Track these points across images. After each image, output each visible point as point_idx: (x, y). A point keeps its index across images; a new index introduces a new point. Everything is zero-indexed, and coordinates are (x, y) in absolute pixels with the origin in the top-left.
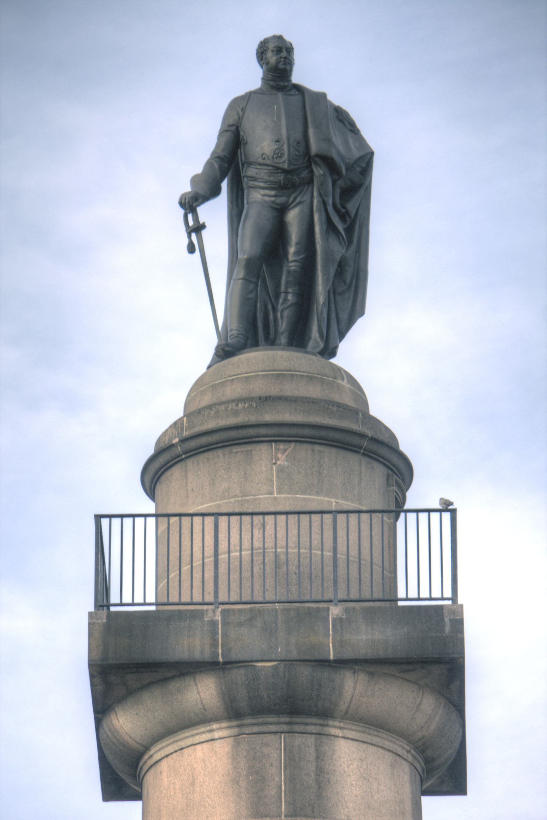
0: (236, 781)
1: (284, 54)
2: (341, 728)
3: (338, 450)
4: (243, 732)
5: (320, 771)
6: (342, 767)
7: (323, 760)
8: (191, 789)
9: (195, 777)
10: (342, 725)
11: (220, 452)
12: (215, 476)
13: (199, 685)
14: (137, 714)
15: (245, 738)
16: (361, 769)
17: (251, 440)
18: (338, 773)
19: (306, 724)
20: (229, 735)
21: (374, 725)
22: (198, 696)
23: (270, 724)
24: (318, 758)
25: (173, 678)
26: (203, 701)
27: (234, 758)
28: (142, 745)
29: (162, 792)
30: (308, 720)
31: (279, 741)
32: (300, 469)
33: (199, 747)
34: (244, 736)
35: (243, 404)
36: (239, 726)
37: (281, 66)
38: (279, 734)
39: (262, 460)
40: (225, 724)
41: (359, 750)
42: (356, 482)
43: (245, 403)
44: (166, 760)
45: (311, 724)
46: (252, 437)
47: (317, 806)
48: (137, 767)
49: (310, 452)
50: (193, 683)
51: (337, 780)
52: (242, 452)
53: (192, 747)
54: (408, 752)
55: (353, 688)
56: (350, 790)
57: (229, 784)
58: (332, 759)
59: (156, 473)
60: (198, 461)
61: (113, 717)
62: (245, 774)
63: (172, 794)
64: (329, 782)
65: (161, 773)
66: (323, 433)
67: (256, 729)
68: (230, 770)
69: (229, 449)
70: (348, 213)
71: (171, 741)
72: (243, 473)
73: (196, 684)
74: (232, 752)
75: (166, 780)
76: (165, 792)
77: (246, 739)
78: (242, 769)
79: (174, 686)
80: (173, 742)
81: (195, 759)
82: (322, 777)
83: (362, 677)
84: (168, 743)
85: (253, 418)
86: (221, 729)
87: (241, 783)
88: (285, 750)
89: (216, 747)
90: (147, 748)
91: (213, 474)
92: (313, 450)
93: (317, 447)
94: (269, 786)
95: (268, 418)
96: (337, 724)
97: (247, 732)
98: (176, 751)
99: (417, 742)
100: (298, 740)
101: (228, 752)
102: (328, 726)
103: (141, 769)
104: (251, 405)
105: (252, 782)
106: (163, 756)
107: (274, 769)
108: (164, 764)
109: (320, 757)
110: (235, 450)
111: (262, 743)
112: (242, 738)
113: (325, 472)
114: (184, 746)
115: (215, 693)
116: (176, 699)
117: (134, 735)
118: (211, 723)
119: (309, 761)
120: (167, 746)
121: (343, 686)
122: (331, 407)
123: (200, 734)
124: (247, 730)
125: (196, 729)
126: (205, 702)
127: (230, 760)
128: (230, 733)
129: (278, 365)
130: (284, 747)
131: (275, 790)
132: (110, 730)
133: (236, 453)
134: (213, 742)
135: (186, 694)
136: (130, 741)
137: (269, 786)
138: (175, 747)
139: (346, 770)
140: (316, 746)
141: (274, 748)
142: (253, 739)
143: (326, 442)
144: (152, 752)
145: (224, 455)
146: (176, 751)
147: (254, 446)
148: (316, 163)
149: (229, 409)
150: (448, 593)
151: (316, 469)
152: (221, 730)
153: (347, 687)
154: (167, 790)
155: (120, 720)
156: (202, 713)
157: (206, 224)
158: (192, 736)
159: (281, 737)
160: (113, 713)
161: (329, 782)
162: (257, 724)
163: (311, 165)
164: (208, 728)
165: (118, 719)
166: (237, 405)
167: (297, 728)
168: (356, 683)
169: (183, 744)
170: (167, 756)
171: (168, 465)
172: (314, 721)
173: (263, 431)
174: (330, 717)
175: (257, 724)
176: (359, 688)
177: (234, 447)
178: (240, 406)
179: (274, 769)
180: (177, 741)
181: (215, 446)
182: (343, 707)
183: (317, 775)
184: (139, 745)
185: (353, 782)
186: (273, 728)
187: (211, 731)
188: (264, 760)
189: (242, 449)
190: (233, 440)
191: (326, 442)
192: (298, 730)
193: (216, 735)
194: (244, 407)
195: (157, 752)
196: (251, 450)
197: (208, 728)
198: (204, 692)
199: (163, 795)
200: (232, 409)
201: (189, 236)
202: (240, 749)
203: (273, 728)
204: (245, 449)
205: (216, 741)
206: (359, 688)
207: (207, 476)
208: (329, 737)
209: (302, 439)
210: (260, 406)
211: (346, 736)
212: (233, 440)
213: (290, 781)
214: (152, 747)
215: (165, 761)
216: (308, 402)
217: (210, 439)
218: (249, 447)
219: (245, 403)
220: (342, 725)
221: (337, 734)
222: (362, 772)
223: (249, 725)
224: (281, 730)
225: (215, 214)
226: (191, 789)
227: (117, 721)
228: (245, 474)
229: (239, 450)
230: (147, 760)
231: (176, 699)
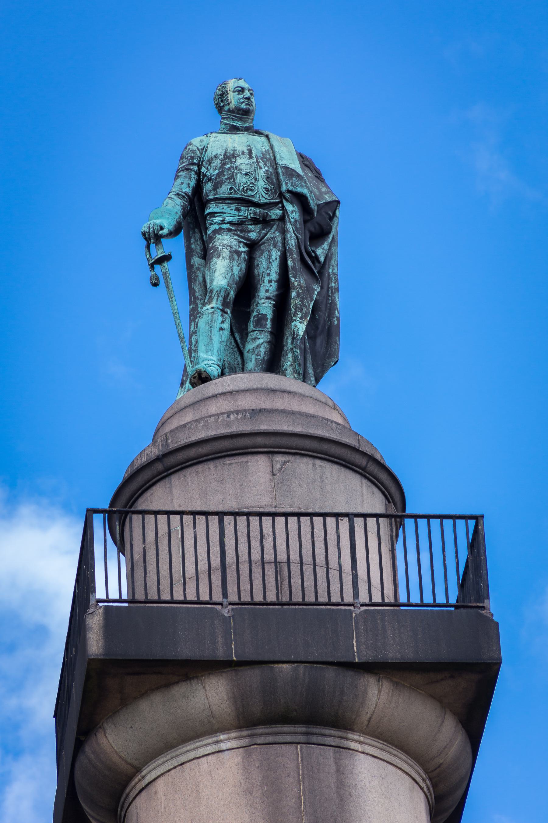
0: (249, 792)
1: (247, 94)
2: (360, 742)
3: (339, 467)
4: (255, 742)
5: (341, 784)
6: (363, 783)
7: (343, 773)
8: (196, 802)
9: (201, 791)
10: (362, 739)
11: (211, 465)
12: (206, 489)
13: (208, 688)
14: (131, 727)
15: (257, 748)
16: (382, 787)
17: (246, 451)
18: (359, 787)
19: (324, 735)
20: (239, 746)
21: (394, 740)
22: (206, 701)
23: (285, 733)
24: (338, 771)
25: (177, 683)
26: (211, 707)
27: (246, 770)
28: (133, 766)
29: (158, 812)
30: (327, 731)
31: (295, 752)
32: (301, 483)
33: (203, 760)
34: (255, 746)
35: (236, 416)
36: (249, 736)
37: (243, 106)
38: (295, 745)
39: (259, 472)
40: (234, 735)
41: (379, 767)
42: (359, 503)
43: (238, 414)
44: (162, 778)
45: (331, 736)
46: (247, 448)
47: (340, 819)
48: (120, 798)
49: (311, 466)
50: (200, 687)
51: (359, 795)
52: (236, 463)
53: (195, 761)
54: (424, 780)
55: (377, 697)
56: (372, 806)
57: (241, 795)
58: (352, 773)
59: (132, 496)
60: (185, 476)
61: (100, 736)
62: (259, 784)
63: (172, 811)
64: (351, 796)
65: (156, 793)
66: (325, 447)
67: (270, 739)
68: (242, 781)
69: (221, 461)
70: (315, 259)
71: (169, 757)
72: (238, 485)
73: (204, 688)
74: (243, 762)
75: (163, 798)
76: (163, 810)
77: (259, 750)
78: (255, 779)
79: (179, 690)
80: (172, 758)
81: (199, 772)
82: (343, 791)
83: (386, 686)
84: (165, 759)
85: (247, 428)
86: (229, 739)
87: (254, 793)
88: (302, 760)
89: (223, 758)
90: (138, 770)
91: (204, 487)
92: (314, 464)
93: (318, 462)
94: (286, 797)
95: (264, 427)
96: (356, 737)
97: (259, 742)
98: (175, 768)
99: (432, 771)
100: (317, 750)
101: (238, 763)
102: (347, 739)
103: (127, 795)
104: (245, 416)
105: (269, 792)
106: (159, 774)
107: (291, 780)
108: (160, 784)
109: (340, 771)
110: (228, 462)
111: (277, 754)
112: (253, 749)
113: (328, 487)
114: (185, 760)
115: (225, 697)
116: (180, 706)
117: (126, 753)
118: (218, 734)
119: (329, 773)
120: (164, 763)
121: (367, 694)
122: (329, 423)
123: (205, 745)
124: (259, 740)
125: (200, 741)
126: (213, 708)
127: (242, 771)
128: (239, 744)
129: (267, 384)
130: (302, 757)
131: (293, 801)
132: (94, 753)
133: (230, 464)
134: (220, 754)
135: (192, 699)
136: (119, 761)
137: (286, 797)
138: (175, 762)
139: (367, 785)
140: (335, 758)
141: (289, 757)
142: (266, 750)
143: (327, 457)
144: (143, 773)
145: (216, 467)
146: (175, 768)
147: (250, 457)
148: (287, 200)
149: (219, 420)
150: (217, 597)
151: (318, 484)
152: (228, 741)
153: (370, 695)
154: (165, 808)
155: (109, 738)
156: (209, 722)
157: (172, 255)
158: (194, 749)
159: (297, 748)
160: (101, 730)
161: (350, 795)
162: (271, 734)
163: (281, 202)
164: (214, 739)
165: (106, 737)
166: (228, 416)
167: (314, 739)
168: (380, 691)
169: (183, 758)
170: (162, 775)
171: (147, 485)
172: (333, 732)
173: (260, 440)
174: (350, 730)
175: (271, 734)
176: (384, 695)
177: (227, 459)
178: (232, 417)
179: (291, 780)
180: (177, 756)
181: (205, 458)
182: (364, 718)
183: (338, 787)
184: (129, 767)
185: (375, 799)
186: (288, 738)
187: (217, 742)
188: (279, 770)
189: (237, 461)
190: (227, 451)
191: (327, 457)
192: (316, 742)
193: (224, 746)
194: (237, 418)
195: (150, 772)
196: (247, 462)
197: (214, 739)
198: (213, 694)
199: (160, 814)
200: (223, 420)
201: (152, 266)
202: (252, 760)
203: (288, 738)
204: (240, 461)
205: (223, 753)
206: (384, 695)
207: (197, 489)
208: (348, 751)
209: (303, 452)
210: (255, 417)
211: (366, 751)
212: (227, 451)
213: (310, 792)
214: (144, 768)
215: (161, 781)
216: (307, 416)
217: (200, 450)
218: (244, 459)
219: (238, 414)
220: (362, 739)
221: (356, 749)
222: (383, 789)
223: (261, 735)
224: (297, 741)
225: (176, 247)
226: (196, 802)
227: (104, 739)
228: (242, 485)
229: (232, 462)
230: (137, 783)
231: (180, 706)
